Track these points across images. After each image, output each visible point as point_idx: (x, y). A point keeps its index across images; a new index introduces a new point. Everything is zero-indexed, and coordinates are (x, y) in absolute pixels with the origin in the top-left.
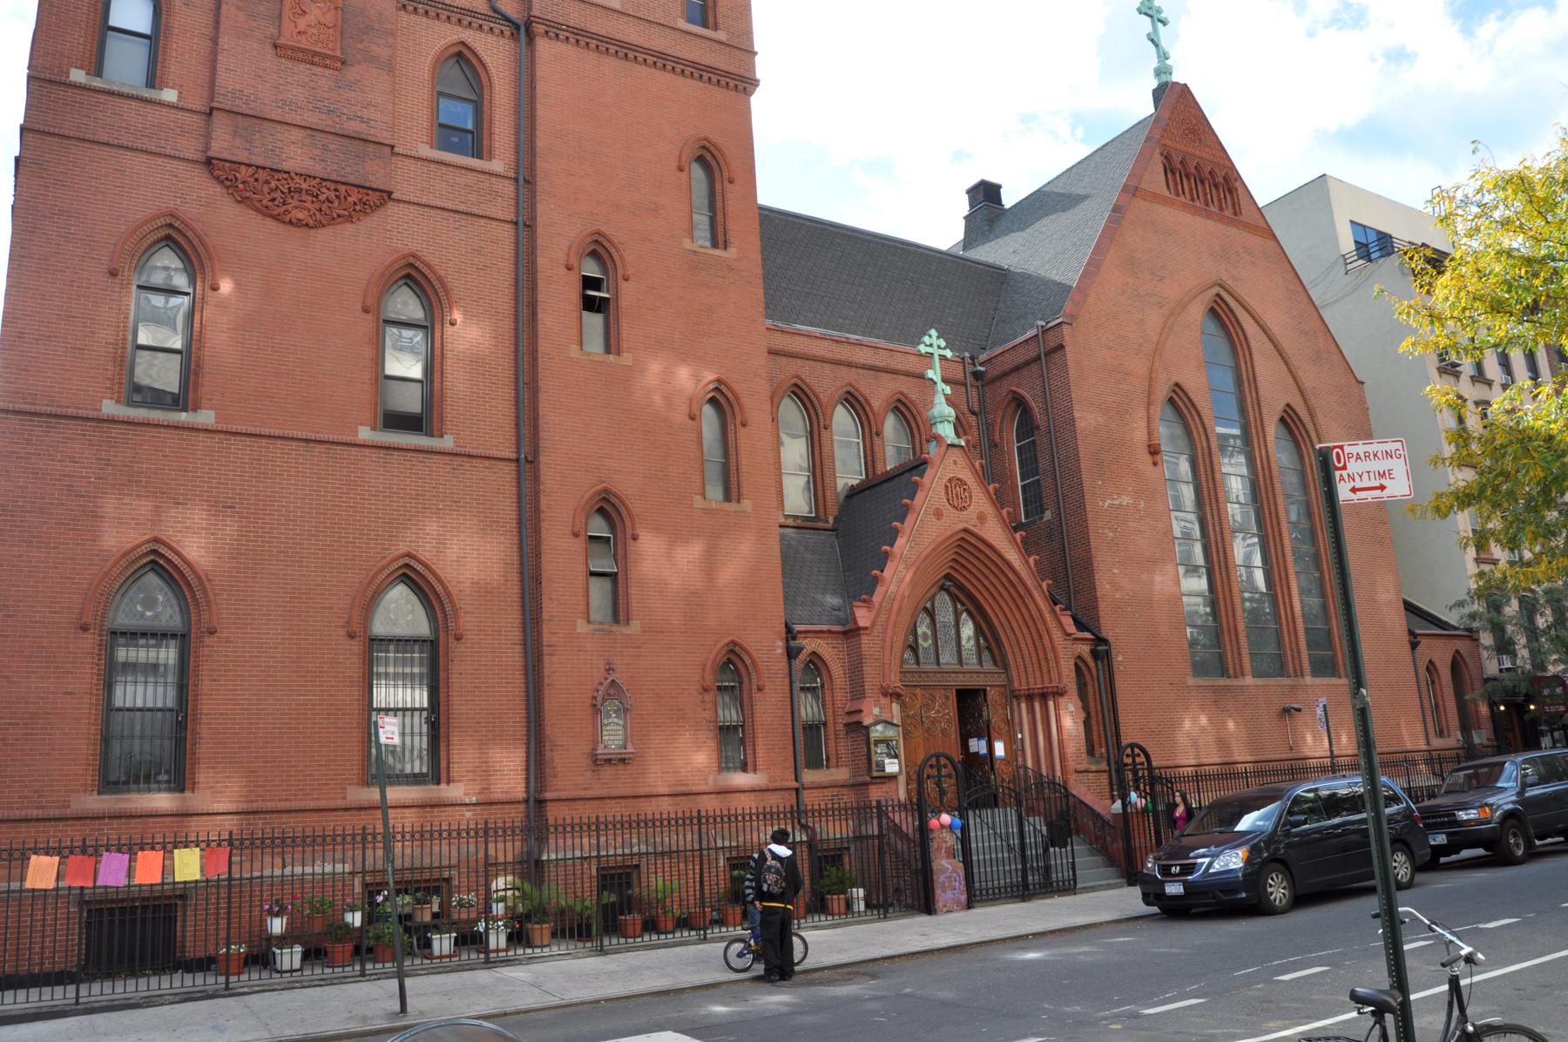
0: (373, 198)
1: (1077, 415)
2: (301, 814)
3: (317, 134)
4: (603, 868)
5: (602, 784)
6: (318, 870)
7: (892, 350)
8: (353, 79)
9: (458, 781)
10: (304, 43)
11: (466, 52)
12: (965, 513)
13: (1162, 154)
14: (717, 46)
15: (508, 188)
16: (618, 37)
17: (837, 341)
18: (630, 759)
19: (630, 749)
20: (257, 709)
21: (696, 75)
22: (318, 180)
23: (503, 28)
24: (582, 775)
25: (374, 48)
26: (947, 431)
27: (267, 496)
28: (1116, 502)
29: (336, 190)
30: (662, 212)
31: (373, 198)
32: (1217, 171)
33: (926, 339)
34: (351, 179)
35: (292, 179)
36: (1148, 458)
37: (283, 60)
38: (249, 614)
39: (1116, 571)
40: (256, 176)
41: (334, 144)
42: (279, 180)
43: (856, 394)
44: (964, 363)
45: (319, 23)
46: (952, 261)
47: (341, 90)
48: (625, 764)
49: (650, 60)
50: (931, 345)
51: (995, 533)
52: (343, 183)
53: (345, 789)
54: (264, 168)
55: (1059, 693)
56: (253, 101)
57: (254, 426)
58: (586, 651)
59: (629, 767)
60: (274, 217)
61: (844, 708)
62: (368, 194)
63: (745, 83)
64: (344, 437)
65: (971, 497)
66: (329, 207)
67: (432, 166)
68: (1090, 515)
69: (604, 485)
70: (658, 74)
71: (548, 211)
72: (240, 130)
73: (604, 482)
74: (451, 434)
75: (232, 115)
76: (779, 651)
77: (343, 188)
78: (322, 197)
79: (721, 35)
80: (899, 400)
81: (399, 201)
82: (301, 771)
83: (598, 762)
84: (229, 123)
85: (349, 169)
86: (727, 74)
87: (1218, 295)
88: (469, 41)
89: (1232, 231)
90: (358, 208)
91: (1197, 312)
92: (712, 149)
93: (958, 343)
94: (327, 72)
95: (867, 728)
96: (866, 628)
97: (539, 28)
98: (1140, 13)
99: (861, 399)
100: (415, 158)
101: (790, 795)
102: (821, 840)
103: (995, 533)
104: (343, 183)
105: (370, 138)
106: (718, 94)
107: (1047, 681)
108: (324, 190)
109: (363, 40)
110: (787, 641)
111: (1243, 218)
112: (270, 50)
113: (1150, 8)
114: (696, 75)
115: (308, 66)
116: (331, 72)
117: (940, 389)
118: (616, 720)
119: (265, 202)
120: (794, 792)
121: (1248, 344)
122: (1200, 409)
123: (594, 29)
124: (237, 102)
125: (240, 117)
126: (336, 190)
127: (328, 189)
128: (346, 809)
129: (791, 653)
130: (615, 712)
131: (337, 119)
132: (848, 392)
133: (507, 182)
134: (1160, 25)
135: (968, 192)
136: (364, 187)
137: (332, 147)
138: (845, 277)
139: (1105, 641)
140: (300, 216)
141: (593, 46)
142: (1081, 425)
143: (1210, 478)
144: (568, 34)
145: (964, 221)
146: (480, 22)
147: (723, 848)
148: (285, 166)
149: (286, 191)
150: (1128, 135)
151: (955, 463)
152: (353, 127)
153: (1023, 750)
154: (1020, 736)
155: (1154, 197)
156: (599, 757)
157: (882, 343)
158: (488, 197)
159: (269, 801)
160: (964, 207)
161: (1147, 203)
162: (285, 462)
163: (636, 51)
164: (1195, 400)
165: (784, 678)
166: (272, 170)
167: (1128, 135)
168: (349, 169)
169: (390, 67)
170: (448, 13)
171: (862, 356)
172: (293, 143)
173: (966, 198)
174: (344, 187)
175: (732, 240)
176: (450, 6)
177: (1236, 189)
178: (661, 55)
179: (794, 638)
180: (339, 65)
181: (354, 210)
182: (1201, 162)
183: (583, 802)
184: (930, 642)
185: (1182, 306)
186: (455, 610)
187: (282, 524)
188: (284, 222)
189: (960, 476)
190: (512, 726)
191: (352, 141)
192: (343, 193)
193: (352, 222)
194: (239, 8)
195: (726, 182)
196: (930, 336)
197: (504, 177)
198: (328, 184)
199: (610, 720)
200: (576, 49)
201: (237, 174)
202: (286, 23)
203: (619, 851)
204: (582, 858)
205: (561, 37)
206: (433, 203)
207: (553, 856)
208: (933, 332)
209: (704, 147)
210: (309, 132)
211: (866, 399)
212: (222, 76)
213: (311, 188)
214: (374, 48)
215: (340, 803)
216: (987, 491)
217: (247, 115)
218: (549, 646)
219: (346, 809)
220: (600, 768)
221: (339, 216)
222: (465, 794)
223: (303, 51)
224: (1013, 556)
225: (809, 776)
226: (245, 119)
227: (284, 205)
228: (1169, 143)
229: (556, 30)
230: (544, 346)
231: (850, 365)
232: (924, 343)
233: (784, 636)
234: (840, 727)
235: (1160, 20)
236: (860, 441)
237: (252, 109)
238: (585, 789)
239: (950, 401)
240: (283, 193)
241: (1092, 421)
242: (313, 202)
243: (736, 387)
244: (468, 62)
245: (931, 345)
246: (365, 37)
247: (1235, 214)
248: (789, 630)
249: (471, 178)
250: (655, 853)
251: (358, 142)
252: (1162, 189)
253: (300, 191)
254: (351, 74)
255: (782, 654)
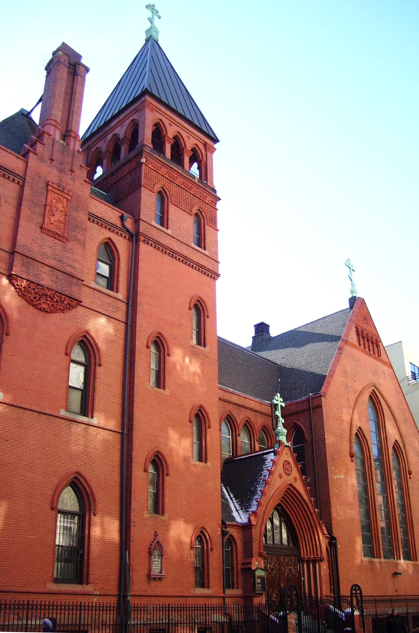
0: (74, 303)
1: (326, 437)
2: (28, 595)
3: (55, 270)
4: (152, 630)
5: (151, 589)
6: (33, 622)
7: (245, 398)
8: (69, 248)
9: (92, 583)
10: (52, 228)
11: (110, 242)
12: (289, 477)
13: (355, 327)
14: (206, 257)
15: (123, 307)
16: (171, 247)
17: (225, 391)
18: (163, 578)
19: (163, 574)
20: (12, 541)
21: (197, 268)
22: (54, 292)
23: (126, 235)
24: (143, 584)
25: (79, 235)
26: (283, 439)
27: (22, 437)
28: (339, 477)
29: (60, 297)
30: (183, 327)
31: (74, 303)
32: (373, 336)
33: (276, 397)
34: (66, 293)
35: (44, 290)
36: (349, 458)
37: (44, 234)
38: (11, 494)
39: (338, 508)
40: (30, 285)
41: (61, 276)
42: (38, 289)
43: (231, 416)
44: (272, 407)
45: (59, 220)
46: (260, 359)
47: (65, 253)
48: (160, 580)
49: (182, 259)
50: (278, 400)
51: (299, 486)
52: (64, 295)
53: (46, 583)
54: (33, 283)
55: (321, 560)
56: (31, 251)
57: (19, 403)
58: (147, 526)
59: (162, 582)
60: (33, 305)
61: (241, 561)
62: (72, 301)
63: (215, 275)
64: (57, 413)
65: (292, 470)
66: (57, 304)
67: (96, 292)
68: (330, 482)
69: (157, 449)
70: (183, 265)
71: (141, 320)
72: (25, 263)
73: (157, 448)
74: (96, 417)
75: (23, 256)
76: (219, 533)
77: (63, 297)
78: (55, 300)
79: (207, 252)
80: (247, 421)
81: (82, 306)
82: (29, 573)
83: (150, 577)
84: (21, 259)
85: (65, 289)
86: (209, 270)
87: (373, 390)
88: (112, 238)
89: (378, 363)
90: (68, 307)
91: (366, 397)
92: (201, 302)
93: (266, 397)
94: (60, 243)
95: (254, 571)
96: (254, 525)
97: (142, 238)
98: (346, 265)
99: (233, 419)
100: (89, 287)
101: (221, 599)
102: (234, 621)
103: (299, 486)
104: (64, 295)
105: (75, 276)
106: (205, 278)
107: (315, 555)
108: (56, 297)
109: (75, 231)
110: (222, 528)
111: (382, 358)
112: (39, 229)
113: (349, 264)
114: (197, 268)
115: (53, 239)
116: (62, 243)
117: (280, 420)
118: (158, 560)
119: (32, 298)
120: (222, 599)
121: (383, 412)
122: (367, 439)
123: (162, 242)
124: (25, 250)
125: (25, 258)
126: (60, 297)
127: (57, 296)
128: (46, 593)
129: (224, 534)
130: (158, 555)
131: (63, 265)
132: (228, 415)
133: (123, 304)
134: (352, 271)
135: (255, 326)
136: (71, 298)
137: (60, 277)
138: (223, 361)
139: (334, 539)
140: (45, 307)
141: (161, 249)
142: (327, 442)
143: (370, 469)
144: (152, 243)
145: (252, 339)
146: (118, 231)
147: (197, 623)
148: (42, 283)
149: (41, 294)
150: (336, 315)
151: (287, 454)
152: (68, 269)
153: (304, 585)
154: (303, 579)
155: (353, 345)
156: (152, 576)
157: (242, 394)
158: (117, 310)
159: (15, 586)
160: (252, 333)
161: (350, 348)
162: (30, 422)
163: (177, 254)
164: (365, 435)
165: (220, 545)
166: (36, 284)
167: (336, 315)
168: (65, 289)
169: (83, 244)
170: (106, 225)
171: (234, 399)
172: (45, 273)
173: (253, 329)
174: (64, 297)
175: (208, 343)
176: (107, 221)
177: (379, 345)
178: (186, 258)
179: (226, 528)
180: (65, 240)
181: (66, 308)
182: (368, 332)
183: (144, 597)
184: (271, 533)
185: (361, 392)
186: (95, 501)
187: (27, 452)
188: (37, 308)
189: (288, 460)
190: (114, 559)
191: (68, 276)
192: (63, 299)
193: (64, 313)
194: (28, 208)
195: (206, 317)
196: (277, 396)
197: (123, 302)
198: (58, 294)
199: (156, 559)
200: (154, 249)
201: (22, 283)
202: (47, 219)
203: (158, 622)
204: (144, 624)
205: (149, 243)
206: (95, 309)
207: (133, 623)
208: (279, 395)
209: (198, 301)
210: (51, 269)
211: (235, 419)
212: (19, 237)
213: (51, 295)
214: (79, 235)
215: (44, 590)
216: (298, 467)
217: (28, 257)
218: (133, 522)
219: (46, 593)
220: (151, 581)
221: (60, 309)
222: (94, 590)
223: (53, 232)
224: (305, 497)
225: (229, 592)
226: (28, 259)
227: (39, 300)
228: (358, 323)
229: (149, 241)
230: (137, 381)
231: (229, 402)
232: (275, 399)
233: (221, 526)
234: (239, 570)
235: (353, 270)
236: (230, 437)
237: (30, 254)
238: (145, 591)
239: (285, 425)
240: (39, 295)
241: (331, 440)
242: (51, 301)
243: (207, 410)
244: (110, 246)
245: (278, 400)
246: (75, 230)
247: (379, 356)
248: (223, 523)
249: (111, 299)
250: (172, 624)
251: (70, 276)
252: (356, 343)
253: (46, 295)
254: (70, 245)
255: (220, 534)
